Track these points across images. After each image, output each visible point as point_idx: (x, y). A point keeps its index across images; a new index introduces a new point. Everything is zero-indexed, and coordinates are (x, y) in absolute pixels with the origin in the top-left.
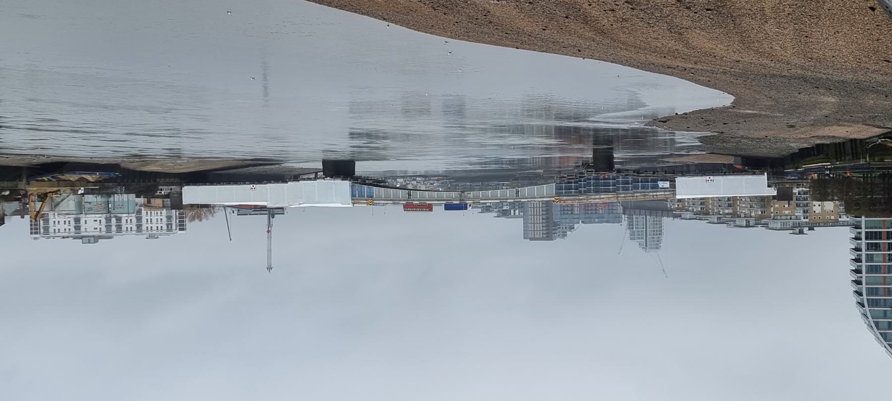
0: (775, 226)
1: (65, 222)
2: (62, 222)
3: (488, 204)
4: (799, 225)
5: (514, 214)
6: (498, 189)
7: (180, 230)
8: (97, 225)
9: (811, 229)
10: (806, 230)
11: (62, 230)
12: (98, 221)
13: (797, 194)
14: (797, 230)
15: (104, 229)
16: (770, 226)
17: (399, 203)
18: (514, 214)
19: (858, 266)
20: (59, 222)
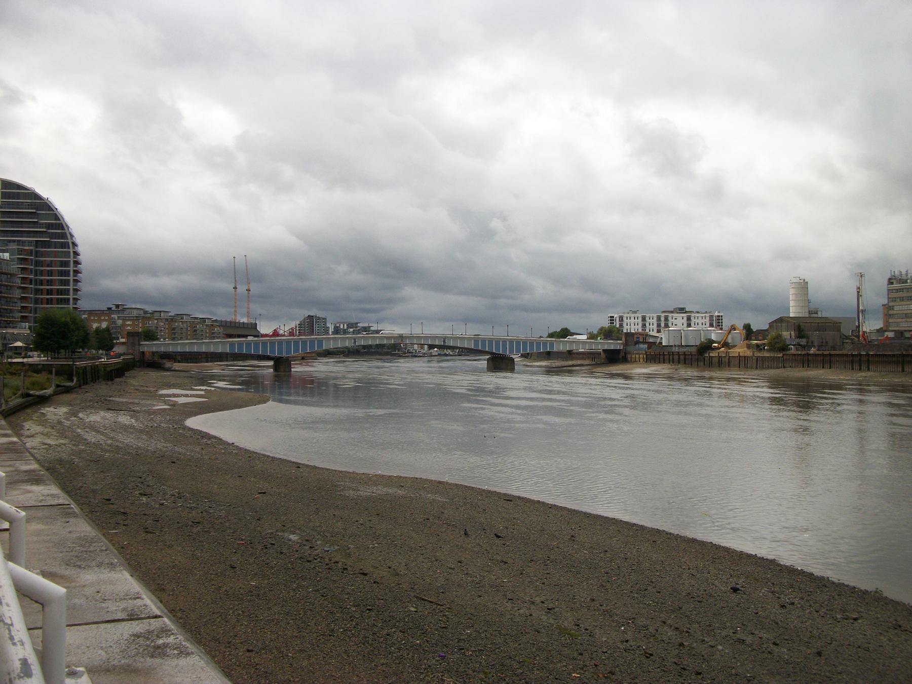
0: (138, 312)
1: (698, 325)
2: (700, 324)
3: (365, 333)
4: (118, 312)
5: (344, 325)
6: (501, 354)
7: (613, 317)
8: (675, 322)
9: (109, 309)
10: (114, 308)
11: (700, 318)
12: (674, 325)
13: (120, 337)
14: (120, 308)
15: (670, 319)
16: (142, 312)
17: (474, 335)
18: (344, 325)
19: (76, 304)
20: (702, 325)
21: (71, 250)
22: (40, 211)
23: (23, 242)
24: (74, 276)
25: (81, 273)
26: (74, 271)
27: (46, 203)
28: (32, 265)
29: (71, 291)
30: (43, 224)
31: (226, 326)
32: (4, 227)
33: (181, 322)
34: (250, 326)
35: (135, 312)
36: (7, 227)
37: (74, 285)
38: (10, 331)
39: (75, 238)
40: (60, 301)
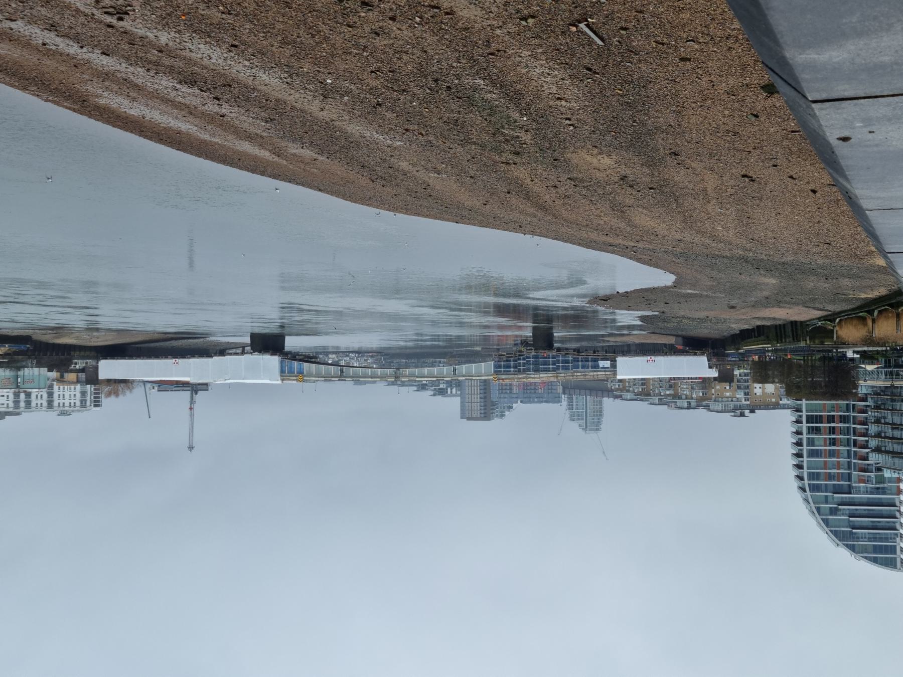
0: (716, 408)
5: (451, 392)
9: (752, 411)
10: (747, 412)
12: (6, 397)
13: (738, 376)
14: (738, 412)
18: (451, 392)
21: (806, 482)
22: (847, 531)
23: (867, 492)
24: (802, 450)
25: (794, 465)
26: (801, 422)
27: (840, 541)
28: (854, 463)
29: (805, 443)
30: (843, 514)
31: (602, 391)
32: (890, 510)
33: (662, 395)
34: (600, 393)
35: (721, 407)
36: (887, 510)
37: (801, 439)
38: (880, 383)
39: (801, 496)
40: (818, 419)
